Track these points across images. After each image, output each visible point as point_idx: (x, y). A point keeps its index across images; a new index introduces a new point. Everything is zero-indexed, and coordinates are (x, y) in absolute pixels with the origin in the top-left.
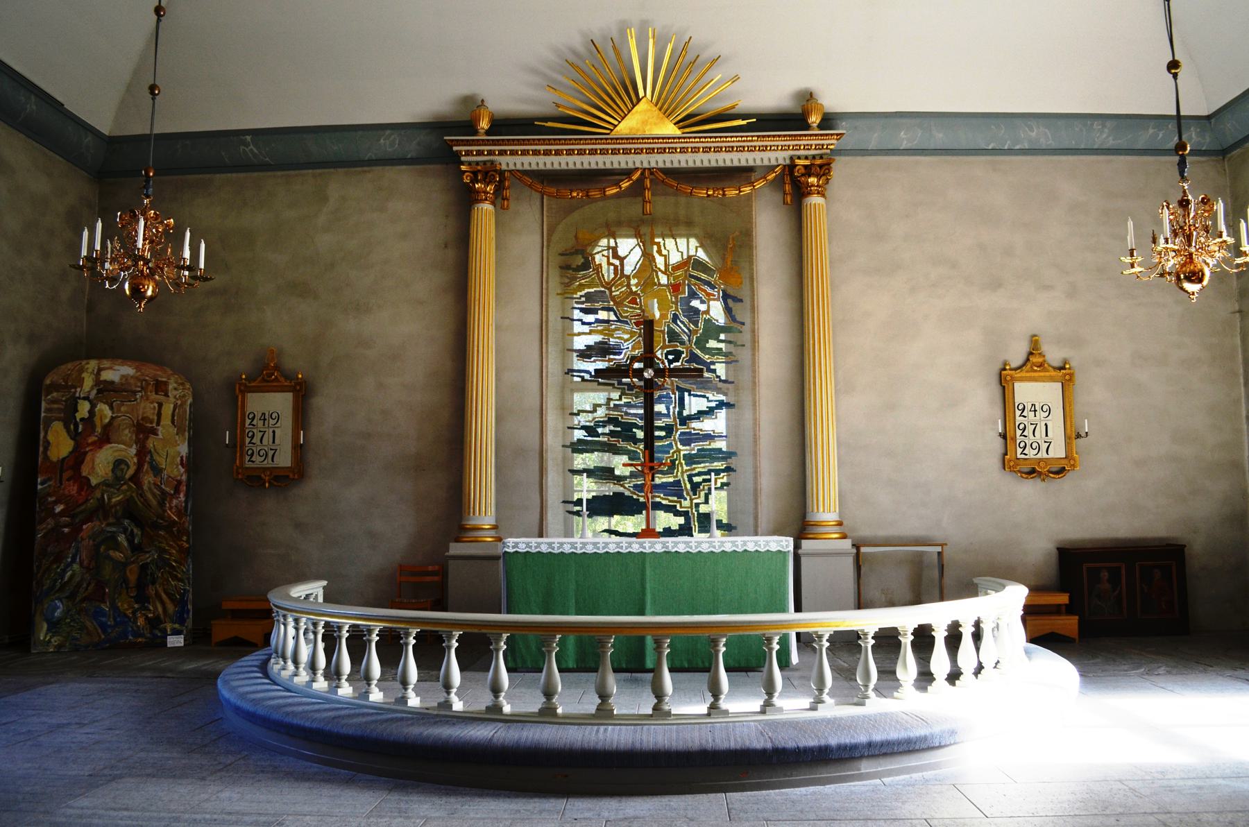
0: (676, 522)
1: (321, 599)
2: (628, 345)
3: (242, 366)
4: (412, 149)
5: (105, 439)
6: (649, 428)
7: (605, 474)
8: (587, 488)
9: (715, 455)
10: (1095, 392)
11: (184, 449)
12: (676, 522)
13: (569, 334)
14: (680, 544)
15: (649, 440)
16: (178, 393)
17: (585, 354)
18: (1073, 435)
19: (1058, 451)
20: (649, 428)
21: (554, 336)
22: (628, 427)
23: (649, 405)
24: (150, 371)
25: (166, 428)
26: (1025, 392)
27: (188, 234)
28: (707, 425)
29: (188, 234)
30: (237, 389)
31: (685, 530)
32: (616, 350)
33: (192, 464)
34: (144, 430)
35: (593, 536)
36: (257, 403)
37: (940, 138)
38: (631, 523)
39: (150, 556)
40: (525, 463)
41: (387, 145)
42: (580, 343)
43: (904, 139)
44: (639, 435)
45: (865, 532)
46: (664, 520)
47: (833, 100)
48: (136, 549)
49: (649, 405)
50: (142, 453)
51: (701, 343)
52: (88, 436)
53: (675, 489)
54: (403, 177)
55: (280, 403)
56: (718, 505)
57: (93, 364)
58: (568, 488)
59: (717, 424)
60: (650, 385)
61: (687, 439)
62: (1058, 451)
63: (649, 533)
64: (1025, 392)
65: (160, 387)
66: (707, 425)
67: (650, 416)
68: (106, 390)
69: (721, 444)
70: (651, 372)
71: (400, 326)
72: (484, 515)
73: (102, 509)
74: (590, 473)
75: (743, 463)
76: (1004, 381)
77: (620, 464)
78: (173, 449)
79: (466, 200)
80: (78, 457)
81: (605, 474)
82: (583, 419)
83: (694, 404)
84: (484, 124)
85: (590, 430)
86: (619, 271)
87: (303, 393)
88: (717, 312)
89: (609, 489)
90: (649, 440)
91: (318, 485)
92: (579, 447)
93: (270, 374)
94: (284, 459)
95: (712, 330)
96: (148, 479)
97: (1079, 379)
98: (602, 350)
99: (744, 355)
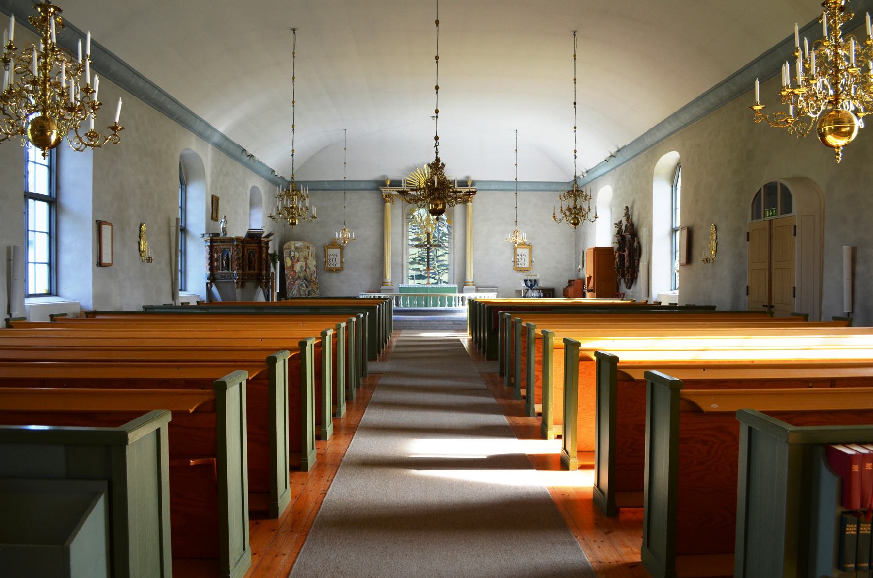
0: (435, 281)
1: (400, 285)
2: (424, 237)
3: (327, 242)
4: (369, 187)
5: (298, 261)
6: (428, 259)
7: (418, 270)
8: (415, 273)
9: (445, 265)
10: (537, 252)
11: (315, 263)
12: (435, 281)
13: (407, 235)
14: (435, 286)
15: (428, 261)
16: (312, 249)
17: (413, 240)
18: (531, 262)
19: (527, 265)
20: (428, 259)
21: (405, 235)
22: (423, 258)
23: (428, 253)
24: (306, 244)
25: (310, 258)
26: (520, 251)
27: (120, 103)
28: (442, 258)
29: (120, 103)
30: (325, 248)
31: (437, 283)
32: (420, 239)
33: (316, 267)
34: (306, 259)
35: (413, 283)
36: (331, 251)
37: (501, 187)
38: (425, 281)
39: (310, 289)
40: (398, 267)
41: (362, 186)
42: (411, 237)
43: (493, 187)
44: (427, 261)
45: (480, 284)
46: (432, 281)
47: (474, 178)
48: (307, 287)
49: (428, 253)
50: (306, 264)
51: (441, 238)
52: (295, 260)
53: (434, 273)
54: (366, 194)
55: (337, 251)
56: (445, 277)
57: (293, 243)
58: (408, 273)
59: (445, 258)
60: (428, 248)
61: (437, 261)
62: (527, 265)
63: (428, 283)
64: (520, 251)
65: (308, 248)
66: (442, 258)
67: (428, 255)
68: (297, 249)
69: (446, 263)
70: (428, 245)
71: (369, 233)
72: (389, 279)
73: (299, 278)
74: (413, 269)
75: (451, 267)
76: (515, 249)
77: (422, 267)
78: (312, 263)
79: (384, 201)
80: (293, 266)
81: (418, 270)
82: (413, 256)
83: (439, 253)
84: (388, 183)
85: (414, 259)
86: (421, 220)
87: (342, 248)
88: (445, 230)
89: (419, 273)
90: (428, 261)
91: (346, 271)
92: (412, 263)
93: (334, 244)
94: (338, 265)
95: (444, 234)
96: (308, 270)
97: (533, 249)
98: (417, 239)
99: (452, 241)
